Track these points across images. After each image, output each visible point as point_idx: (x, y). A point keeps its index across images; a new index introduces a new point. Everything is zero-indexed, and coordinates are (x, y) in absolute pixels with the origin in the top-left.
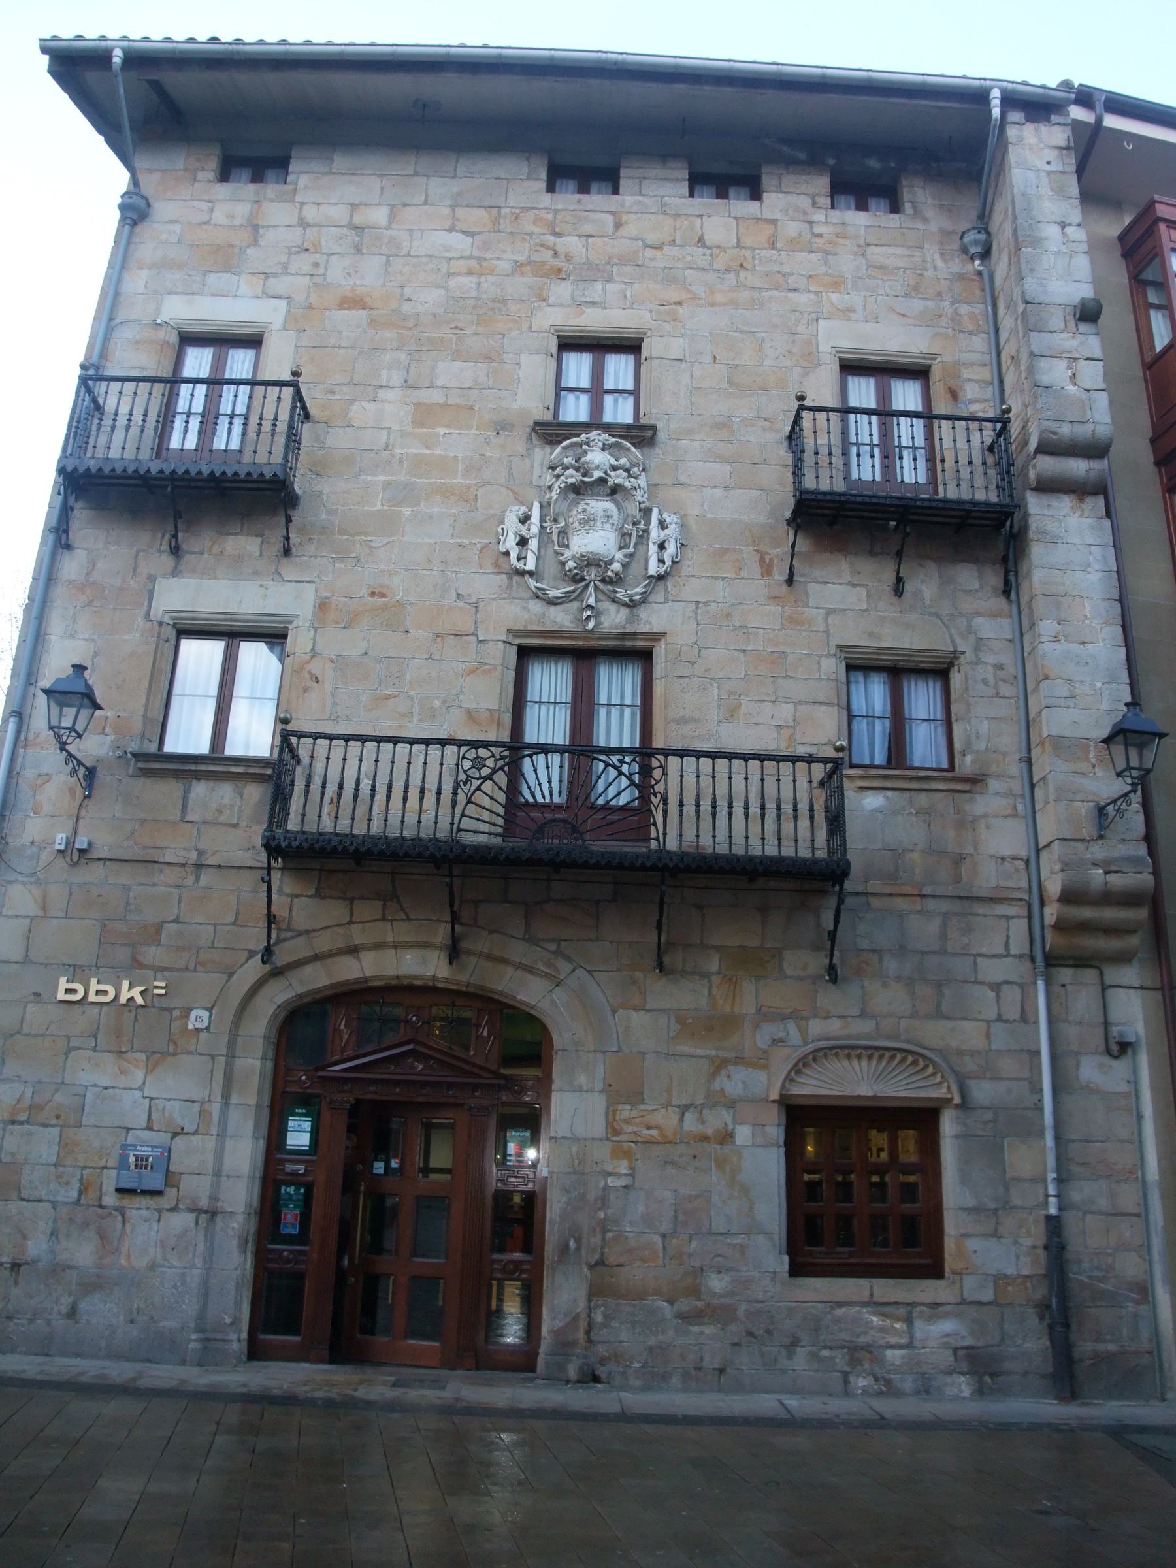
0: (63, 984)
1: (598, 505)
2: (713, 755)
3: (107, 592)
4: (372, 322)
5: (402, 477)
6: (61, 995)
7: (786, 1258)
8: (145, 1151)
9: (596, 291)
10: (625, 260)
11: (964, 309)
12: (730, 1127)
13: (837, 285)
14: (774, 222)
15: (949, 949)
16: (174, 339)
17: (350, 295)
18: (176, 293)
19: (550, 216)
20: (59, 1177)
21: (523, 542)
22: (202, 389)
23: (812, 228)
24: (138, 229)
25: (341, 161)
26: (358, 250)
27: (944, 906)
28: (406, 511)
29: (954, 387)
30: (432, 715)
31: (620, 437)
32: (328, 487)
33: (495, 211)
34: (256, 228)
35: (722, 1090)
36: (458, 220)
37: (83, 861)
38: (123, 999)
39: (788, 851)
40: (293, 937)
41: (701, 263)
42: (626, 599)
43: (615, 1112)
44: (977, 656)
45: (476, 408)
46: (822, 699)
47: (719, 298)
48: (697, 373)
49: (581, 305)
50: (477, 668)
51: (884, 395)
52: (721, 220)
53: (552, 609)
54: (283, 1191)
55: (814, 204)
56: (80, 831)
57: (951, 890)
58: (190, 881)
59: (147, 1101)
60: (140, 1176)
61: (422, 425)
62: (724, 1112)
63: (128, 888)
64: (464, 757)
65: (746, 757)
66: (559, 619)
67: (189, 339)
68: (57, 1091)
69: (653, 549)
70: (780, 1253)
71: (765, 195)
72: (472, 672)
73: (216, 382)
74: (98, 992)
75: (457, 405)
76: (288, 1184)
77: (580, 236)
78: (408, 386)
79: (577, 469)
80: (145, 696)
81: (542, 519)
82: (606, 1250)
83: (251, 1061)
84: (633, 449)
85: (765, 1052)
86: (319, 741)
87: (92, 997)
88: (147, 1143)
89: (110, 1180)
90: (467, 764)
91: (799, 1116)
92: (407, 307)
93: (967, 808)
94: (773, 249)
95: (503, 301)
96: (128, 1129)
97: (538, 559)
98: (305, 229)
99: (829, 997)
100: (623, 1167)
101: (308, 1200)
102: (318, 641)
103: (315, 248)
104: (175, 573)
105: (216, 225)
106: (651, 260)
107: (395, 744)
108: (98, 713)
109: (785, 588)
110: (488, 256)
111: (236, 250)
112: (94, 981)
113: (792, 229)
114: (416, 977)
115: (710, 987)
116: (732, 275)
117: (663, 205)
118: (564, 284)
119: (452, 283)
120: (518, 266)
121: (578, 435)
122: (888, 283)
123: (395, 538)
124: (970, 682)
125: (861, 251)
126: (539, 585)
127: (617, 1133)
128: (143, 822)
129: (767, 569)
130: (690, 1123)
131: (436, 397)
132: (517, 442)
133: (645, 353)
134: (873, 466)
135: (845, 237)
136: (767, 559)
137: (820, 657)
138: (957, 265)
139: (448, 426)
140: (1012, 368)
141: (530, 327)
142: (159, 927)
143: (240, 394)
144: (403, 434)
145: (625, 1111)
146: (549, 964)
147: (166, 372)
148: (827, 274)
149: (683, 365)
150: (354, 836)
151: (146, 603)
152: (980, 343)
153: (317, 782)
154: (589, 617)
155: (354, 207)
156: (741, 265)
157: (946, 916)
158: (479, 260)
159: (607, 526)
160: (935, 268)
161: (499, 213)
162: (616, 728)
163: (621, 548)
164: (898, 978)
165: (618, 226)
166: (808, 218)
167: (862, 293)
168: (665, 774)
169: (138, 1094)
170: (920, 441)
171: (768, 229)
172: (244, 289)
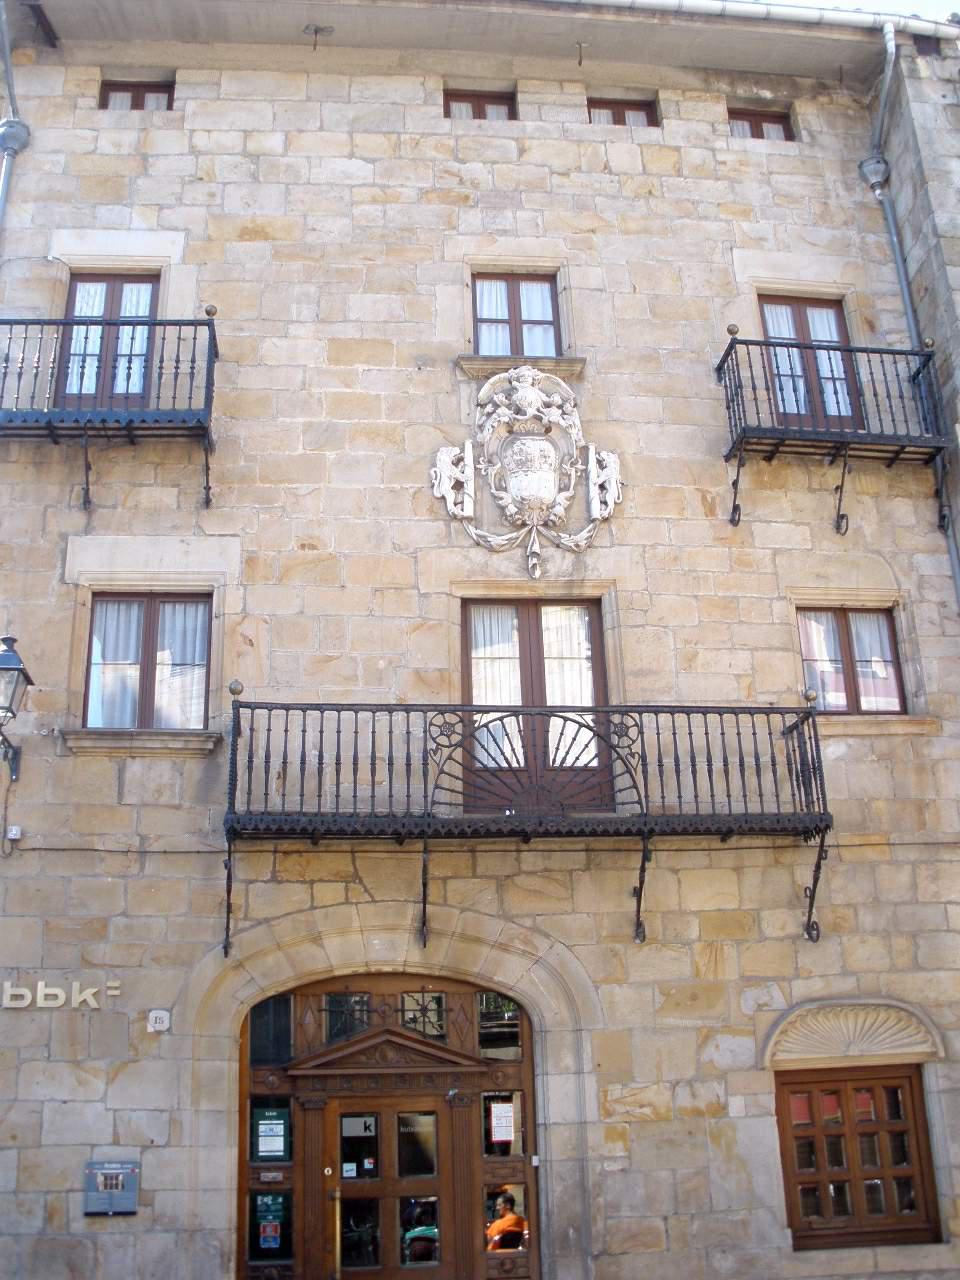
0: (8, 989)
1: (534, 446)
2: (672, 710)
3: (15, 554)
4: (277, 254)
5: (323, 418)
6: (7, 1002)
7: (789, 1232)
8: (112, 1169)
9: (506, 219)
10: (533, 186)
11: (871, 238)
12: (722, 1099)
13: (746, 213)
14: (677, 149)
15: (920, 899)
16: (65, 276)
17: (250, 226)
18: (65, 227)
19: (452, 142)
20: (20, 1205)
21: (458, 486)
22: (96, 331)
23: (714, 156)
24: (20, 158)
25: (229, 84)
26: (255, 178)
27: (913, 854)
28: (331, 455)
29: (869, 317)
30: (379, 678)
31: (549, 371)
32: (241, 431)
33: (394, 137)
34: (145, 158)
35: (711, 1061)
36: (357, 146)
37: (16, 853)
38: (75, 1003)
39: (754, 808)
40: (252, 927)
41: (612, 189)
42: (572, 545)
43: (606, 1092)
44: (920, 594)
45: (395, 342)
46: (776, 643)
47: (632, 226)
48: (618, 303)
49: (492, 235)
50: (422, 625)
51: (801, 324)
52: (626, 146)
53: (495, 556)
54: (259, 1202)
55: (714, 131)
56: (11, 818)
57: (918, 837)
58: (135, 869)
59: (111, 1114)
60: (111, 1196)
61: (337, 362)
62: (715, 1084)
63: (69, 880)
64: (431, 724)
65: (705, 711)
66: (503, 569)
67: (79, 276)
68: (10, 1108)
69: (594, 491)
70: (783, 1228)
71: (665, 121)
72: (417, 628)
73: (111, 323)
74: (47, 997)
75: (374, 340)
76: (265, 1193)
77: (484, 163)
78: (319, 320)
79: (508, 407)
80: (66, 668)
81: (476, 461)
82: (608, 1238)
83: (218, 1063)
84: (563, 384)
85: (751, 1018)
86: (258, 711)
87: (41, 1002)
88: (112, 1157)
89: (76, 1204)
90: (435, 731)
91: (789, 1082)
92: (311, 238)
93: (926, 751)
94: (679, 176)
95: (411, 230)
96: (93, 1146)
97: (475, 503)
98: (197, 158)
99: (810, 957)
100: (618, 1149)
101: (287, 1207)
102: (249, 600)
103: (211, 177)
104: (88, 530)
105: (102, 154)
106: (559, 186)
107: (356, 712)
108: (29, 687)
109: (730, 527)
110: (391, 183)
111: (127, 180)
112: (41, 985)
113: (695, 155)
114: (386, 963)
115: (692, 955)
116: (642, 202)
117: (565, 131)
118: (472, 212)
119: (356, 211)
120: (424, 193)
121: (507, 370)
122: (795, 212)
123: (322, 485)
124: (917, 620)
125: (766, 178)
126: (479, 532)
127: (609, 1114)
128: (78, 807)
129: (710, 511)
130: (684, 1098)
131: (349, 332)
132: (443, 376)
133: (561, 283)
134: (838, 403)
135: (748, 165)
136: (709, 497)
137: (772, 599)
138: (861, 194)
139: (367, 362)
140: (926, 299)
141: (443, 257)
142: (104, 923)
143: (91, 336)
144: (319, 371)
145: (616, 1091)
146: (526, 942)
147: (59, 315)
148: (734, 202)
149: (604, 295)
150: (323, 815)
151: (59, 564)
152: (888, 272)
153: (260, 754)
154: (534, 565)
155: (247, 134)
156: (650, 192)
157: (914, 864)
158: (383, 187)
159: (546, 466)
160: (838, 196)
161: (399, 138)
162: (569, 682)
163: (561, 490)
164: (874, 932)
165: (522, 151)
166: (710, 145)
167: (772, 222)
168: (641, 732)
169: (100, 1106)
170: (839, 372)
171: (674, 157)
172: (137, 222)
